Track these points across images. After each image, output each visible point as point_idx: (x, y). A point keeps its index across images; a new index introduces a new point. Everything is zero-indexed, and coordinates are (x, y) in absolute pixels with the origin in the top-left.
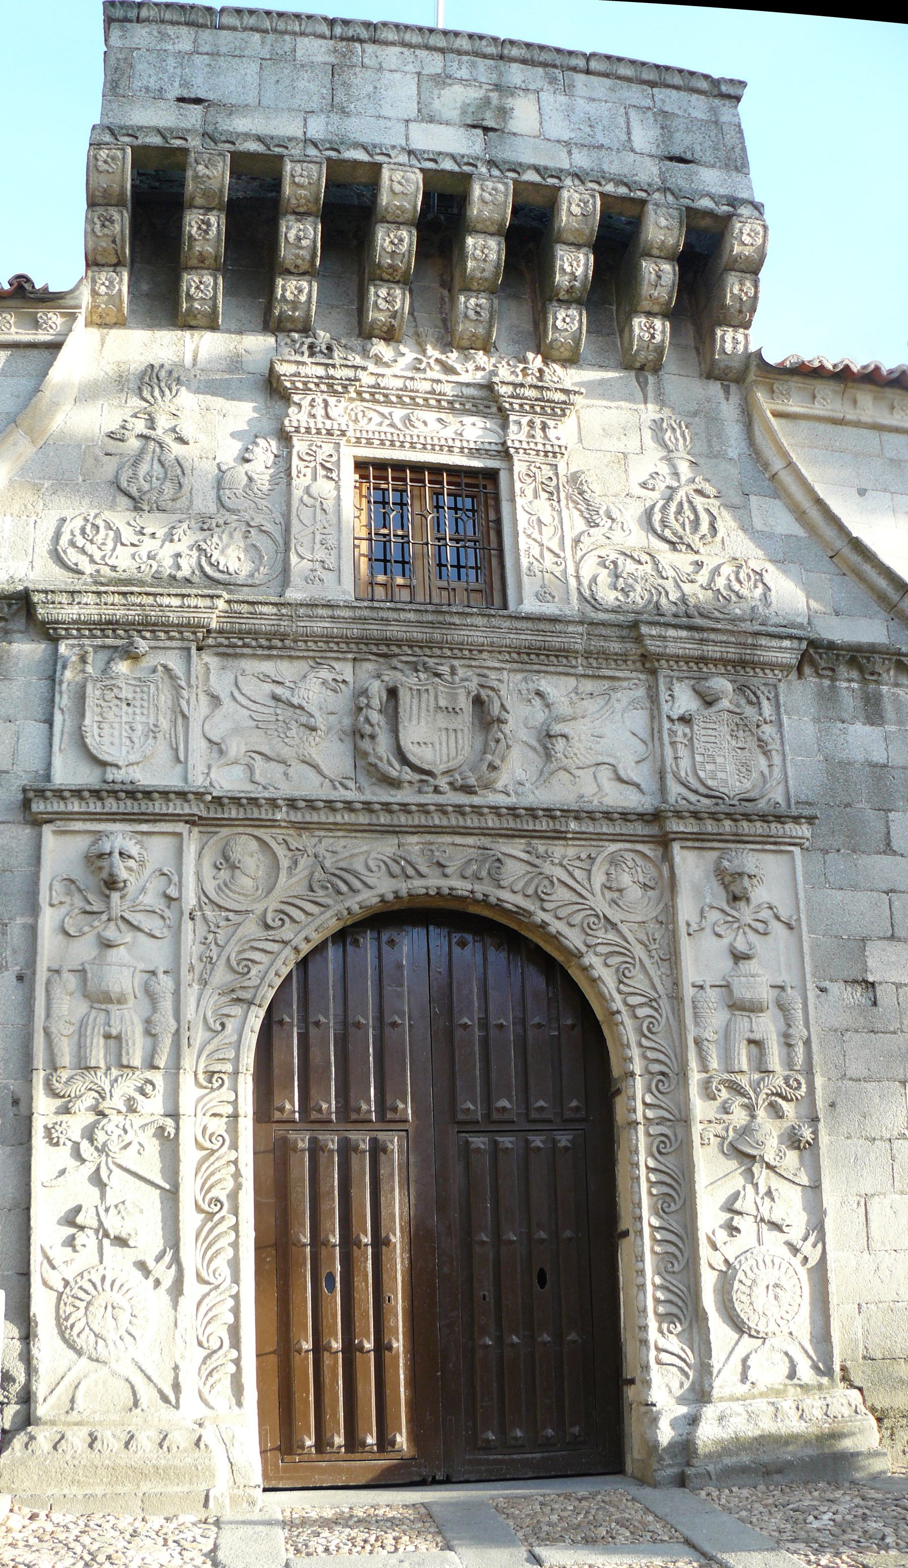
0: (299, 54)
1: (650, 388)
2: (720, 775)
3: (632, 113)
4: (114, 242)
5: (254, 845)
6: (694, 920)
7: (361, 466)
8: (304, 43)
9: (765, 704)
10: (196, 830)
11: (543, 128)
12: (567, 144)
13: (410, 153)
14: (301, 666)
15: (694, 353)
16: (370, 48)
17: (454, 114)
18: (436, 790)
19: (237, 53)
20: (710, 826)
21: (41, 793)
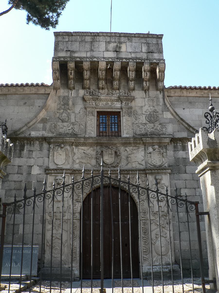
1: (147, 94)
7: (98, 112)
8: (87, 37)
11: (127, 50)
12: (131, 52)
13: (104, 58)
14: (88, 147)
15: (155, 86)
16: (98, 37)
17: (111, 49)
19: (76, 40)
20: (153, 171)
21: (47, 170)
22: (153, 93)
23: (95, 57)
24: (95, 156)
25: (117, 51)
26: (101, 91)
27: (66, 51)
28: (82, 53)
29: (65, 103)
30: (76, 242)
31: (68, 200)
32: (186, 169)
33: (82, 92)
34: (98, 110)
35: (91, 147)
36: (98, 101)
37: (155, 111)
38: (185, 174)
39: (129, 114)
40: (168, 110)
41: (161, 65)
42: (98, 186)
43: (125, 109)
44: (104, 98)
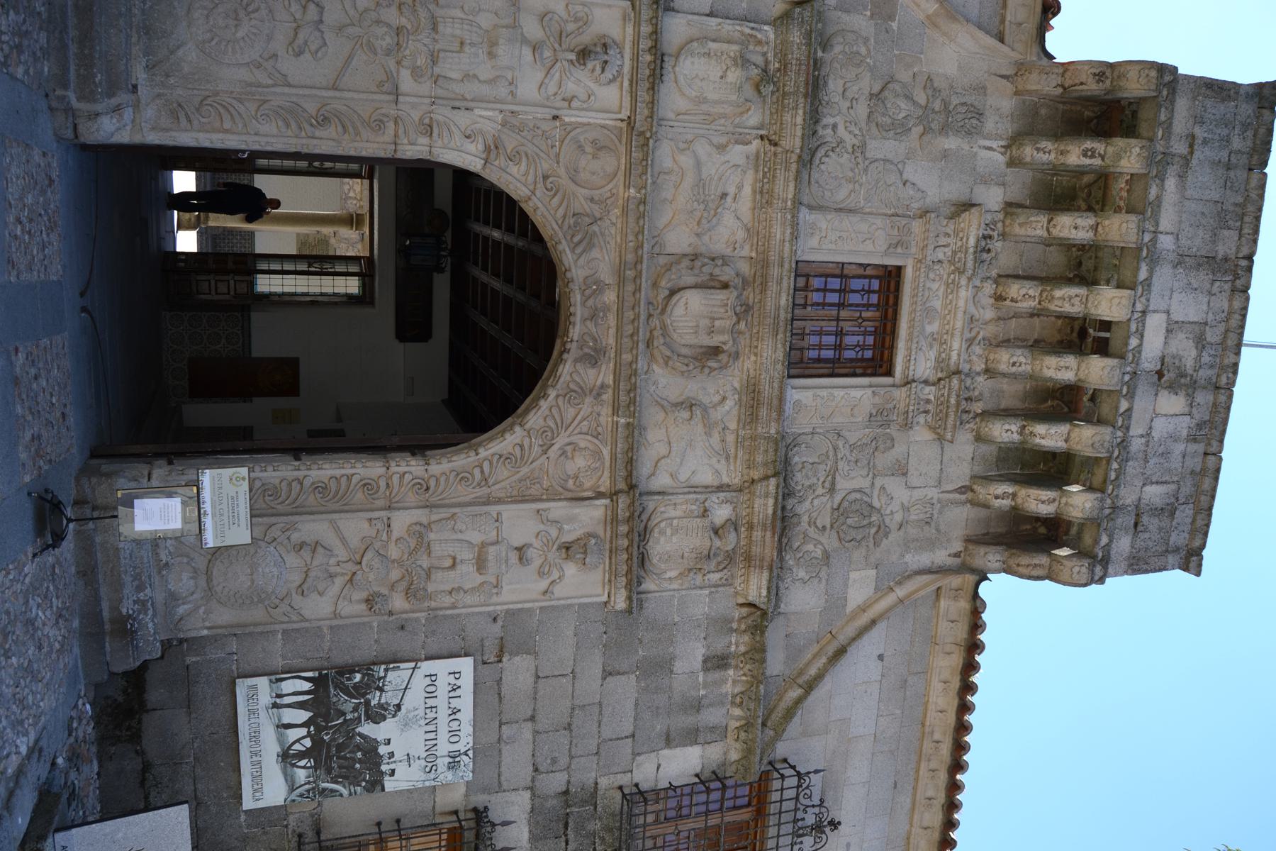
0: (1226, 232)
1: (957, 496)
2: (662, 539)
3: (1173, 487)
4: (1082, 84)
5: (610, 169)
6: (553, 515)
9: (718, 576)
10: (624, 125)
11: (1164, 414)
13: (1144, 312)
16: (1227, 287)
18: (650, 316)
22: (960, 519)
23: (1151, 272)
24: (703, 249)
25: (1160, 374)
26: (989, 288)
27: (1193, 137)
28: (1177, 211)
29: (952, 114)
30: (275, 131)
31: (497, 101)
32: (623, 678)
33: (993, 198)
34: (909, 273)
35: (748, 230)
36: (949, 275)
37: (882, 531)
38: (597, 671)
39: (880, 417)
40: (882, 589)
41: (1080, 568)
42: (561, 261)
43: (904, 395)
44: (961, 303)
